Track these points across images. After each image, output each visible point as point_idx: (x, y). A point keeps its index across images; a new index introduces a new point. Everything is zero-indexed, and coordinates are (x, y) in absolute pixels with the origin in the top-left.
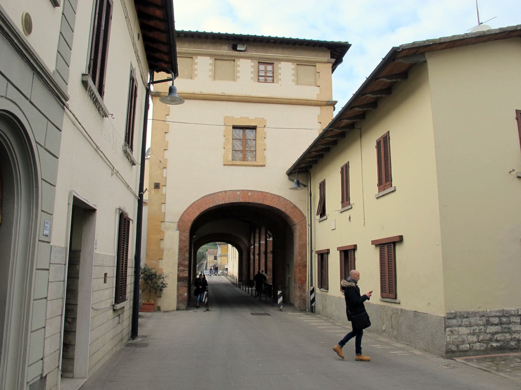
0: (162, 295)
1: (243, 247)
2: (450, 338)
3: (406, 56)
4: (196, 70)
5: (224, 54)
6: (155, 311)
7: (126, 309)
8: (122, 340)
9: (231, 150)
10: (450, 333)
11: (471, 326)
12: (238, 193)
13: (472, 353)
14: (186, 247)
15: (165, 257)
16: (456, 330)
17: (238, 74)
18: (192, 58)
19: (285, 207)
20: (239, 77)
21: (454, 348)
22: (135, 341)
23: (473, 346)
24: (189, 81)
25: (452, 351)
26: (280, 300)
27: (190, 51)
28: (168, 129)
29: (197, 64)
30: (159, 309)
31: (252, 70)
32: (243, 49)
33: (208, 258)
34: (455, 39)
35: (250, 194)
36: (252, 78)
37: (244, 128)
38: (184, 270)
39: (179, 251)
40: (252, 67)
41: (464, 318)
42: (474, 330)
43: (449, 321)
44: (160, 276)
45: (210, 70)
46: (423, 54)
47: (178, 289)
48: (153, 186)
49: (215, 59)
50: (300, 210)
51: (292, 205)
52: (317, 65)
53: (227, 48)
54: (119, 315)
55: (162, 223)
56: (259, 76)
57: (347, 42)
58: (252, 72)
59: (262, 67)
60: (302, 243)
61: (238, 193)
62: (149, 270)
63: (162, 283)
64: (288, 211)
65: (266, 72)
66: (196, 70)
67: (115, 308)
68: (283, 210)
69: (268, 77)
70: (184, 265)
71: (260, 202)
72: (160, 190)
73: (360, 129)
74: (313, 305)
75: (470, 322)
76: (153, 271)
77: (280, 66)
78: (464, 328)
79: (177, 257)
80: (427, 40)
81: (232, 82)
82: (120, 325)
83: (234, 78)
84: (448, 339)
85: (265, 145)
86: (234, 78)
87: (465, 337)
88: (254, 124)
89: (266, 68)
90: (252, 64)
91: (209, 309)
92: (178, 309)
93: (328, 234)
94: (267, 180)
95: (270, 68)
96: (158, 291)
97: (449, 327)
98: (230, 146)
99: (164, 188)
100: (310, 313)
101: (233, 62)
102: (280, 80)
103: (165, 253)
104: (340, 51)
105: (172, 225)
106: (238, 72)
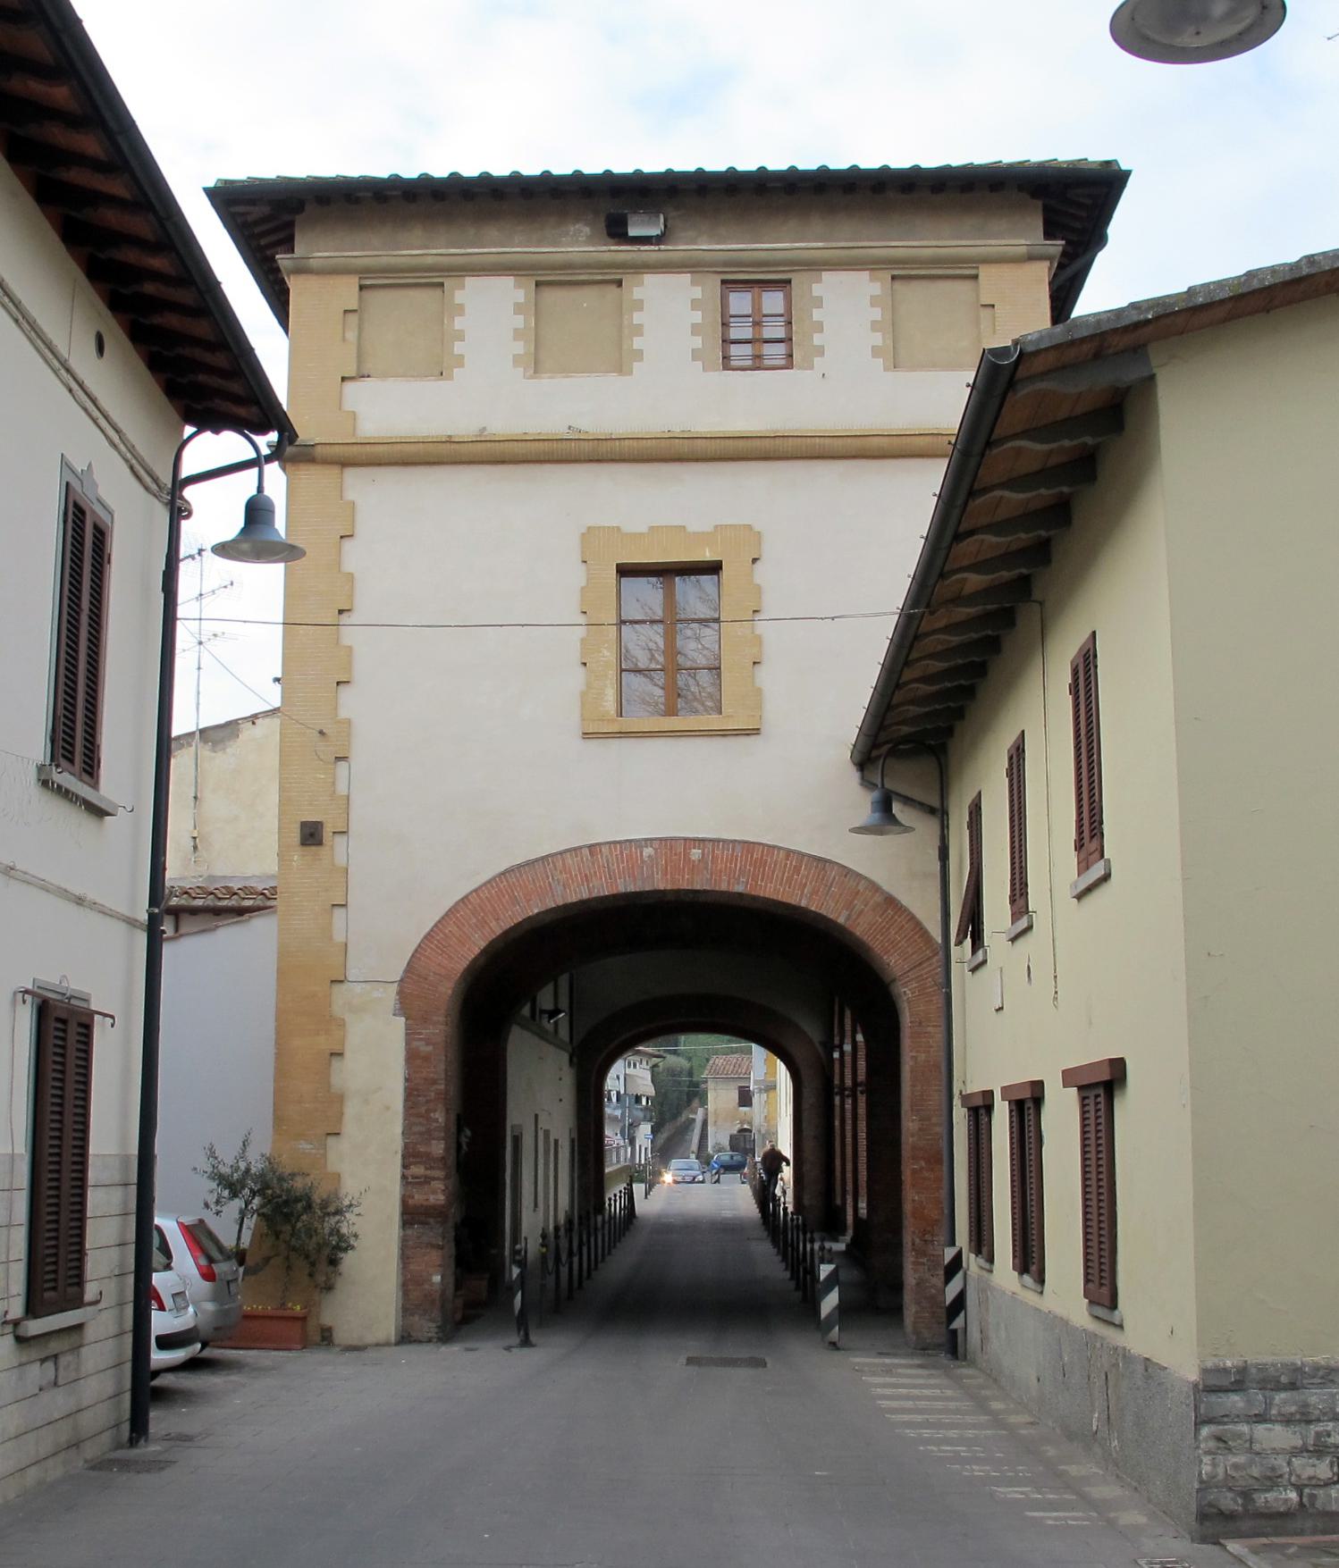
0: (340, 1284)
1: (800, 1054)
2: (1214, 1465)
3: (1060, 369)
4: (460, 336)
5: (576, 258)
6: (305, 1344)
7: (90, 1333)
8: (75, 1444)
9: (612, 673)
10: (1212, 1444)
11: (1309, 1422)
12: (648, 851)
13: (1309, 1524)
14: (434, 1082)
15: (349, 1126)
16: (1240, 1435)
17: (637, 343)
18: (442, 285)
19: (849, 906)
20: (639, 355)
21: (1229, 1502)
22: (134, 1453)
23: (1313, 1497)
24: (431, 387)
25: (1221, 1513)
26: (830, 1302)
27: (430, 260)
28: (351, 596)
29: (460, 310)
30: (326, 1337)
31: (697, 317)
32: (654, 231)
33: (710, 1096)
34: (1256, 284)
35: (696, 853)
36: (696, 355)
37: (666, 572)
38: (427, 1180)
39: (406, 1100)
40: (695, 304)
41: (1279, 1387)
42: (1318, 1435)
43: (1213, 1398)
44: (325, 1205)
45: (518, 334)
46: (1137, 351)
47: (405, 1258)
48: (295, 836)
49: (538, 284)
50: (912, 918)
51: (878, 898)
52: (984, 272)
53: (587, 230)
54: (56, 1357)
55: (336, 987)
56: (727, 342)
57: (1108, 163)
58: (696, 330)
59: (740, 302)
60: (923, 1056)
61: (648, 851)
62: (281, 1179)
63: (336, 1231)
64: (862, 925)
65: (757, 324)
66: (460, 336)
67: (21, 1332)
68: (841, 920)
69: (767, 341)
70: (425, 1159)
71: (739, 888)
72: (323, 851)
73: (1041, 603)
74: (958, 1323)
75: (1306, 1405)
76: (299, 1184)
77: (817, 289)
78: (1278, 1427)
79: (397, 1128)
80: (1133, 306)
81: (613, 378)
82: (56, 1390)
83: (620, 360)
84: (1206, 1469)
85: (758, 641)
86: (620, 360)
87: (1280, 1462)
88: (708, 555)
89: (757, 305)
90: (697, 292)
91: (533, 1338)
92: (405, 1338)
93: (1007, 1025)
94: (769, 789)
95: (773, 302)
96: (323, 1266)
97: (1210, 1421)
98: (609, 655)
99: (339, 839)
100: (943, 1358)
101: (613, 288)
102: (820, 351)
103: (351, 1109)
104: (1088, 202)
105: (376, 994)
106: (638, 329)
